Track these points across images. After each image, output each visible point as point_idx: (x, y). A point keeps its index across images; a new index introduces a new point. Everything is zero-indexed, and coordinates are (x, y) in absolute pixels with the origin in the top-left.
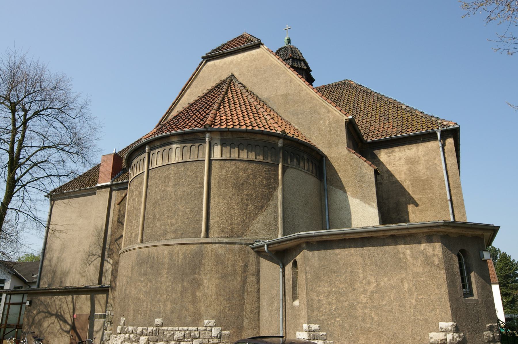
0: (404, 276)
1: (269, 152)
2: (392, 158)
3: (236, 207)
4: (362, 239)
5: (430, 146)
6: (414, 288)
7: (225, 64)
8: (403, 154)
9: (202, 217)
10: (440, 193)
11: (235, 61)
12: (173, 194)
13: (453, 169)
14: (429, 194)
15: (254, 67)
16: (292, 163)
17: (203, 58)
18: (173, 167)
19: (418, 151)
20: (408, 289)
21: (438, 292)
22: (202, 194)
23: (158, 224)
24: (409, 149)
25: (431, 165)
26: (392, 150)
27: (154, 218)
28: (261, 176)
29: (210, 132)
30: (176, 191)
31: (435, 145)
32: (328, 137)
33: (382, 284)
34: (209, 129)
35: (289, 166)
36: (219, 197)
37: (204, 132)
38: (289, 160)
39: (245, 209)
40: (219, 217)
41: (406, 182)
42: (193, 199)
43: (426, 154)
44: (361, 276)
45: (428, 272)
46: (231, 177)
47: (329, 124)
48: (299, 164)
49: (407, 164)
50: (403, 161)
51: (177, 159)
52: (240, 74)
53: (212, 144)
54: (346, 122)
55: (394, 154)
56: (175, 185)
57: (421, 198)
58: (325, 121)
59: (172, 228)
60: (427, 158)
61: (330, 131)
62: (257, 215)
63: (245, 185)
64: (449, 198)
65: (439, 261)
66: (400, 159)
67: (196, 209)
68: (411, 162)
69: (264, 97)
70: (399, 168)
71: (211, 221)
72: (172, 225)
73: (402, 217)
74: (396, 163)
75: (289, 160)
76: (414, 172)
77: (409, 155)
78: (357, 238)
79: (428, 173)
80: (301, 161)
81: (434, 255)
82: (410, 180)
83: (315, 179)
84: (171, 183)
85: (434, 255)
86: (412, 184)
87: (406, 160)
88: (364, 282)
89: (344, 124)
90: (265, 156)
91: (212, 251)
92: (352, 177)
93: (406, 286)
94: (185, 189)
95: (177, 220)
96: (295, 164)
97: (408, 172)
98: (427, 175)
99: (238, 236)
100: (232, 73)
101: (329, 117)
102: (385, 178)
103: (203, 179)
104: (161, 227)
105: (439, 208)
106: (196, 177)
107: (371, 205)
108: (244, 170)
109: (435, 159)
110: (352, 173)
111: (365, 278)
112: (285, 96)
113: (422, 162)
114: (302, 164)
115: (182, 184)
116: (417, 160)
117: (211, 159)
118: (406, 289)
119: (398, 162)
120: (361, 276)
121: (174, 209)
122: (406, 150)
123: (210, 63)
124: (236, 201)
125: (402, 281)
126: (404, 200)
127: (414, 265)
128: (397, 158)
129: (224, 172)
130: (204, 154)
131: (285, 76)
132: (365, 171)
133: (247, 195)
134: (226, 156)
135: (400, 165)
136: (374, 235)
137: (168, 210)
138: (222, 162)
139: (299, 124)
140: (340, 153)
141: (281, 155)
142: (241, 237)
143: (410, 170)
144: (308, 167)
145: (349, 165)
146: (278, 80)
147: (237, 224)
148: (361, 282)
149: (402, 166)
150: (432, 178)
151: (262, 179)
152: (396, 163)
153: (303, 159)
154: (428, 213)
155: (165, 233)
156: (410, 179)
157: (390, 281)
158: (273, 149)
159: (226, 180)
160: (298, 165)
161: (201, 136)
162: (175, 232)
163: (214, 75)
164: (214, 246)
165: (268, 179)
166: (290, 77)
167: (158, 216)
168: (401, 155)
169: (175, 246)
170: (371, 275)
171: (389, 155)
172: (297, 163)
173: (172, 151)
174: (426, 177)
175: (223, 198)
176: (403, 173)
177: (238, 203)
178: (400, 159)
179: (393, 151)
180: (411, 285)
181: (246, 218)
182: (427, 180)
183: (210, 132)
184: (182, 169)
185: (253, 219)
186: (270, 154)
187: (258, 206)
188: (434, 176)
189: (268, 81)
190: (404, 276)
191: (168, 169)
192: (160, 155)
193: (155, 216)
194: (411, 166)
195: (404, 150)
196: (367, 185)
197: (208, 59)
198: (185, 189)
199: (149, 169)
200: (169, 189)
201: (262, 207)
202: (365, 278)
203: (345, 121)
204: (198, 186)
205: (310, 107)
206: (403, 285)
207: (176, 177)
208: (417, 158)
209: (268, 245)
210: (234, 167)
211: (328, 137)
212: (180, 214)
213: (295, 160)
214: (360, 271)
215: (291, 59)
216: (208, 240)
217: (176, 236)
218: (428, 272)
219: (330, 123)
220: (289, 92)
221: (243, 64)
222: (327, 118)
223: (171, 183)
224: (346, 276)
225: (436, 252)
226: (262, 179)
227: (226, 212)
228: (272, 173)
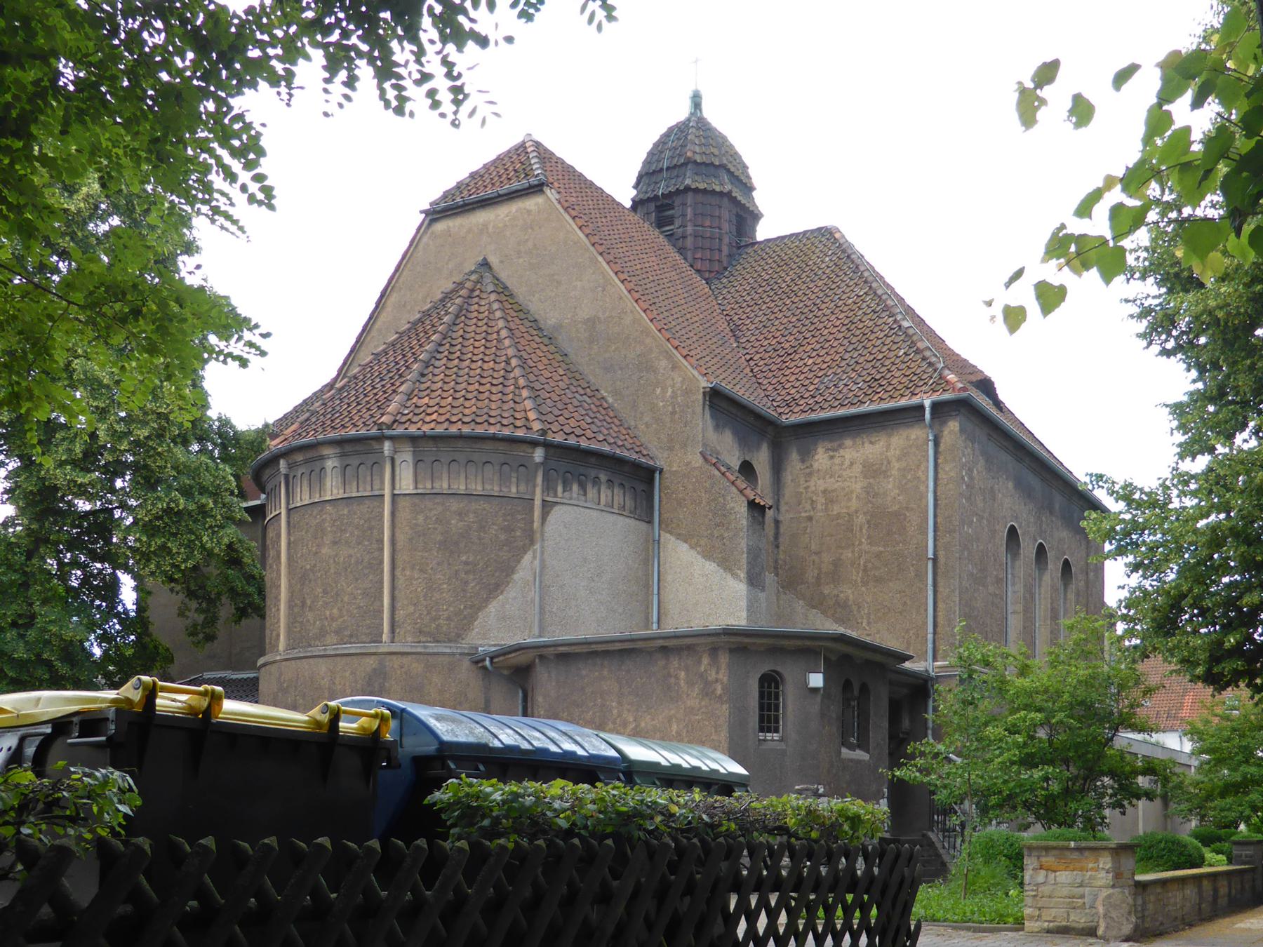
0: (673, 712)
1: (514, 475)
2: (837, 461)
3: (445, 586)
4: (621, 651)
5: (913, 437)
6: (685, 731)
7: (470, 231)
8: (859, 455)
9: (383, 606)
10: (918, 544)
11: (492, 224)
12: (332, 561)
13: (949, 490)
14: (898, 544)
15: (530, 244)
16: (566, 494)
17: (426, 212)
18: (329, 508)
19: (888, 447)
20: (677, 732)
21: (715, 738)
22: (381, 562)
23: (310, 616)
24: (871, 443)
25: (909, 480)
26: (838, 443)
27: (303, 606)
28: (493, 524)
29: (391, 438)
30: (336, 556)
31: (917, 434)
32: (668, 425)
33: (643, 724)
34: (387, 432)
35: (558, 500)
36: (413, 568)
37: (380, 439)
38: (560, 489)
39: (464, 591)
40: (415, 605)
41: (858, 517)
42: (366, 571)
43: (904, 455)
44: (615, 712)
45: (706, 707)
46: (436, 529)
47: (672, 397)
48: (585, 495)
49: (865, 477)
50: (858, 468)
51: (335, 491)
52: (502, 262)
53: (398, 462)
54: (704, 393)
55: (842, 452)
56: (335, 543)
57: (881, 552)
58: (664, 390)
59: (334, 625)
60: (904, 464)
61: (673, 413)
62: (487, 601)
63: (462, 545)
64: (930, 555)
65: (723, 689)
66: (852, 464)
67: (373, 590)
68: (873, 471)
69: (549, 322)
70: (849, 484)
71: (400, 614)
72: (333, 619)
73: (842, 592)
74: (844, 473)
75: (560, 489)
76: (876, 495)
77: (871, 456)
78: (614, 651)
79: (901, 498)
80: (589, 486)
81: (717, 681)
82: (865, 514)
83: (632, 522)
84: (328, 539)
85: (717, 681)
86: (868, 522)
87: (864, 467)
88: (618, 721)
89: (700, 397)
90: (504, 480)
91: (402, 667)
92: (706, 516)
93: (675, 727)
94: (351, 552)
95: (340, 610)
96: (575, 495)
97: (864, 495)
98: (900, 502)
99: (450, 641)
100: (485, 259)
101: (673, 380)
102: (819, 507)
103: (383, 533)
104: (315, 622)
105: (913, 574)
106: (371, 528)
107: (735, 576)
108: (460, 514)
109: (918, 467)
110: (707, 508)
111: (620, 715)
112: (592, 322)
113: (894, 472)
114: (592, 492)
115: (346, 542)
116: (884, 468)
117: (396, 492)
118: (674, 733)
119: (848, 472)
120: (615, 712)
121: (335, 590)
122: (866, 445)
123: (440, 227)
124: (444, 575)
125: (669, 721)
126: (850, 555)
127: (688, 695)
128: (847, 463)
129: (421, 518)
130: (382, 482)
131: (594, 273)
132: (732, 505)
133: (466, 563)
134: (425, 487)
135: (850, 477)
136: (640, 645)
137: (325, 592)
138: (416, 500)
139: (616, 393)
140: (689, 463)
141: (539, 480)
142: (456, 641)
143: (868, 490)
144: (610, 498)
145: (703, 491)
146: (579, 283)
147: (448, 619)
148: (614, 723)
149: (853, 480)
150: (907, 508)
151: (496, 530)
152: (844, 473)
153: (596, 481)
154: (891, 584)
155: (322, 633)
156: (865, 510)
157: (653, 720)
158: (521, 468)
159: (424, 535)
160: (583, 498)
161: (376, 446)
162: (337, 632)
163: (449, 260)
164: (406, 660)
165: (508, 530)
166: (604, 277)
167: (309, 602)
168: (855, 455)
169: (339, 658)
170: (629, 711)
171: (831, 454)
172: (582, 492)
173: (325, 472)
174: (897, 507)
175: (421, 570)
176: (854, 496)
177: (449, 579)
178: (852, 464)
179: (840, 446)
180: (681, 726)
181: (465, 607)
182: (896, 514)
183: (391, 438)
184: (346, 512)
185: (480, 609)
186: (514, 480)
187: (489, 585)
188: (912, 505)
189: (559, 283)
190: (673, 712)
191: (321, 511)
192: (305, 483)
193: (304, 603)
194: (872, 480)
195: (863, 443)
196: (731, 534)
197: (435, 217)
198: (351, 552)
199: (292, 506)
200: (325, 550)
201: (497, 586)
202: (620, 715)
203: (702, 390)
204: (375, 546)
205: (638, 353)
206: (670, 727)
207: (334, 529)
208: (885, 463)
209: (492, 659)
210: (440, 509)
211: (668, 425)
212: (346, 599)
213: (575, 487)
214: (614, 704)
215: (689, 167)
216: (395, 648)
217: (342, 639)
218: (706, 707)
219: (674, 396)
220: (600, 315)
221: (508, 234)
222: (669, 382)
223: (328, 539)
224: (594, 713)
225: (721, 676)
226: (496, 530)
227: (425, 596)
228: (519, 517)
